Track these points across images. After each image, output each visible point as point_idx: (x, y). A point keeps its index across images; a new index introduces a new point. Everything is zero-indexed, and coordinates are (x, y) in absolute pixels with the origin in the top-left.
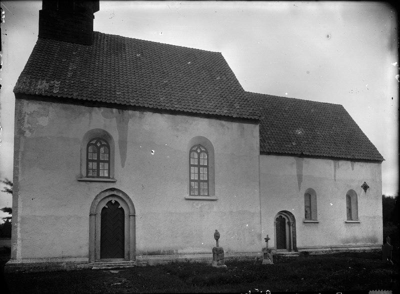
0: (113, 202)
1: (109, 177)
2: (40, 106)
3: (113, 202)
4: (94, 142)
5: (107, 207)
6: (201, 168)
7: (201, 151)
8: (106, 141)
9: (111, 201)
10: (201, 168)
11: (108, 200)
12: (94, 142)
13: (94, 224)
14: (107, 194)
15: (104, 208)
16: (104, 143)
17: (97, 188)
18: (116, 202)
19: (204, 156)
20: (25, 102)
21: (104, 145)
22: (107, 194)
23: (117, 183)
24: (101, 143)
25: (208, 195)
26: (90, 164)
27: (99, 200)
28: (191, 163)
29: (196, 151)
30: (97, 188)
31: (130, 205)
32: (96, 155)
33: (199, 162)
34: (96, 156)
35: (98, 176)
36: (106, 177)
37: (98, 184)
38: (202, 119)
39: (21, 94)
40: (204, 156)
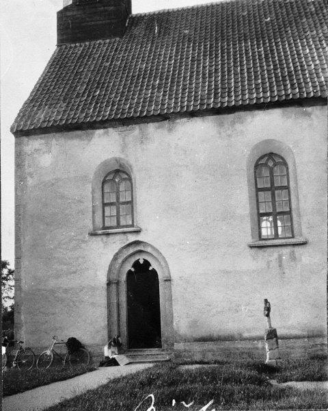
0: (141, 262)
1: (132, 226)
2: (43, 141)
3: (141, 262)
4: (263, 161)
5: (133, 270)
6: (276, 192)
7: (275, 165)
8: (127, 174)
9: (137, 262)
10: (276, 192)
11: (133, 260)
12: (263, 161)
13: (115, 315)
14: (131, 250)
15: (130, 271)
16: (278, 160)
17: (116, 244)
18: (145, 261)
19: (282, 172)
20: (25, 139)
21: (125, 179)
22: (131, 250)
23: (142, 233)
24: (274, 160)
25: (293, 237)
26: (107, 209)
27: (120, 261)
28: (259, 187)
29: (266, 165)
30: (116, 244)
31: (162, 263)
32: (129, 217)
33: (272, 183)
34: (115, 211)
35: (118, 226)
36: (127, 226)
37: (118, 237)
38: (270, 110)
39: (21, 132)
40: (282, 172)
